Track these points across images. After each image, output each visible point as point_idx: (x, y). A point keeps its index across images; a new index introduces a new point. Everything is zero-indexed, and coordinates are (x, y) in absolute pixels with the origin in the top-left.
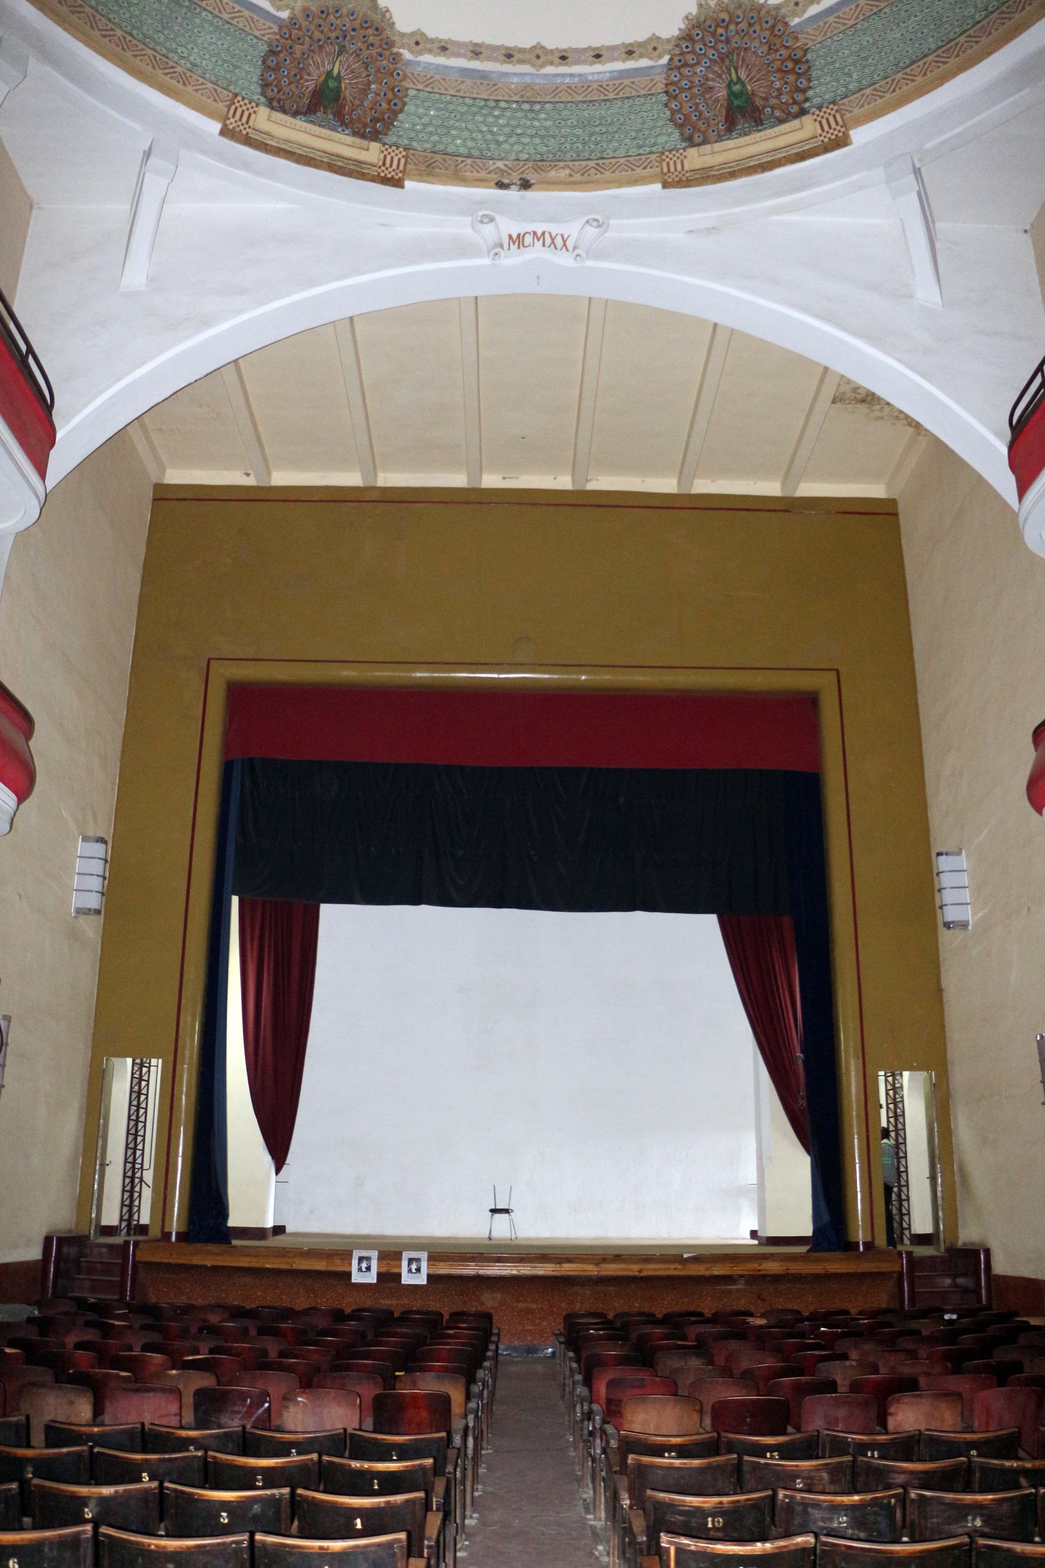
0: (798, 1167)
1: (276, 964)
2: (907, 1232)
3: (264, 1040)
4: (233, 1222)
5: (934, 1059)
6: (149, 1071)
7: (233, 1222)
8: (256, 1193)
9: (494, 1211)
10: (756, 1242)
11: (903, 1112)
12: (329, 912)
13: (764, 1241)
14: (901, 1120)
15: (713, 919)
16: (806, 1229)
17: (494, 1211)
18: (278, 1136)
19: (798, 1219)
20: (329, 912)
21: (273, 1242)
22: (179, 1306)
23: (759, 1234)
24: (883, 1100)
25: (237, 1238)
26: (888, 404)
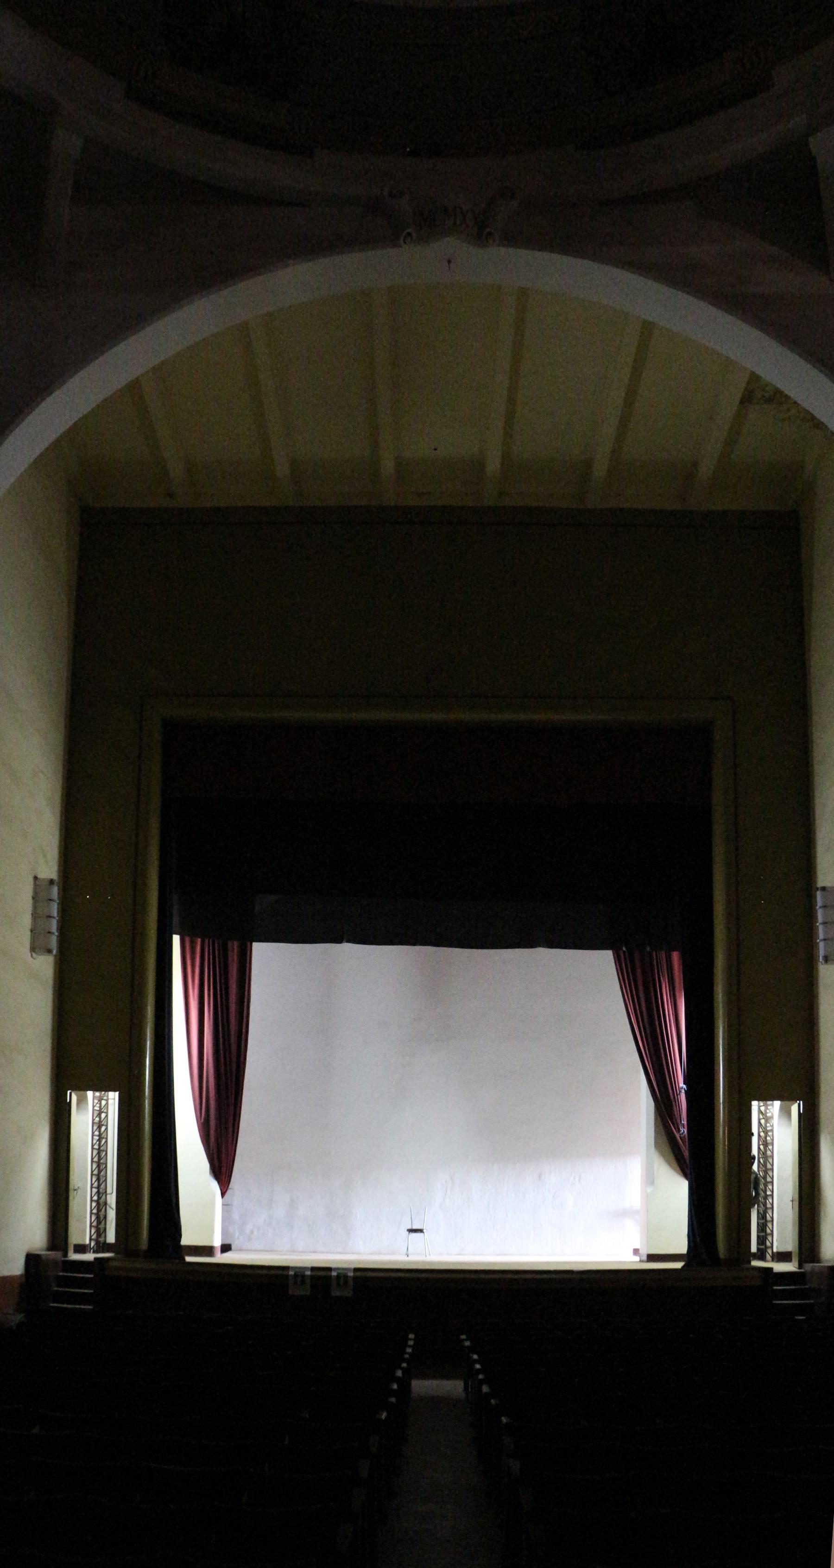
0: (677, 1191)
1: (215, 1006)
2: (770, 1251)
3: (207, 1072)
4: (185, 1241)
5: (801, 1086)
6: (107, 1103)
7: (185, 1241)
8: (205, 1214)
9: (411, 1231)
10: (637, 1259)
11: (773, 1140)
12: (255, 945)
13: (645, 1258)
14: (771, 1160)
15: (607, 956)
16: (682, 1248)
17: (411, 1231)
18: (222, 1167)
19: (678, 1242)
20: (255, 945)
21: (220, 1258)
22: (140, 1315)
23: (641, 1252)
24: (755, 1151)
25: (190, 1255)
26: (795, 403)
